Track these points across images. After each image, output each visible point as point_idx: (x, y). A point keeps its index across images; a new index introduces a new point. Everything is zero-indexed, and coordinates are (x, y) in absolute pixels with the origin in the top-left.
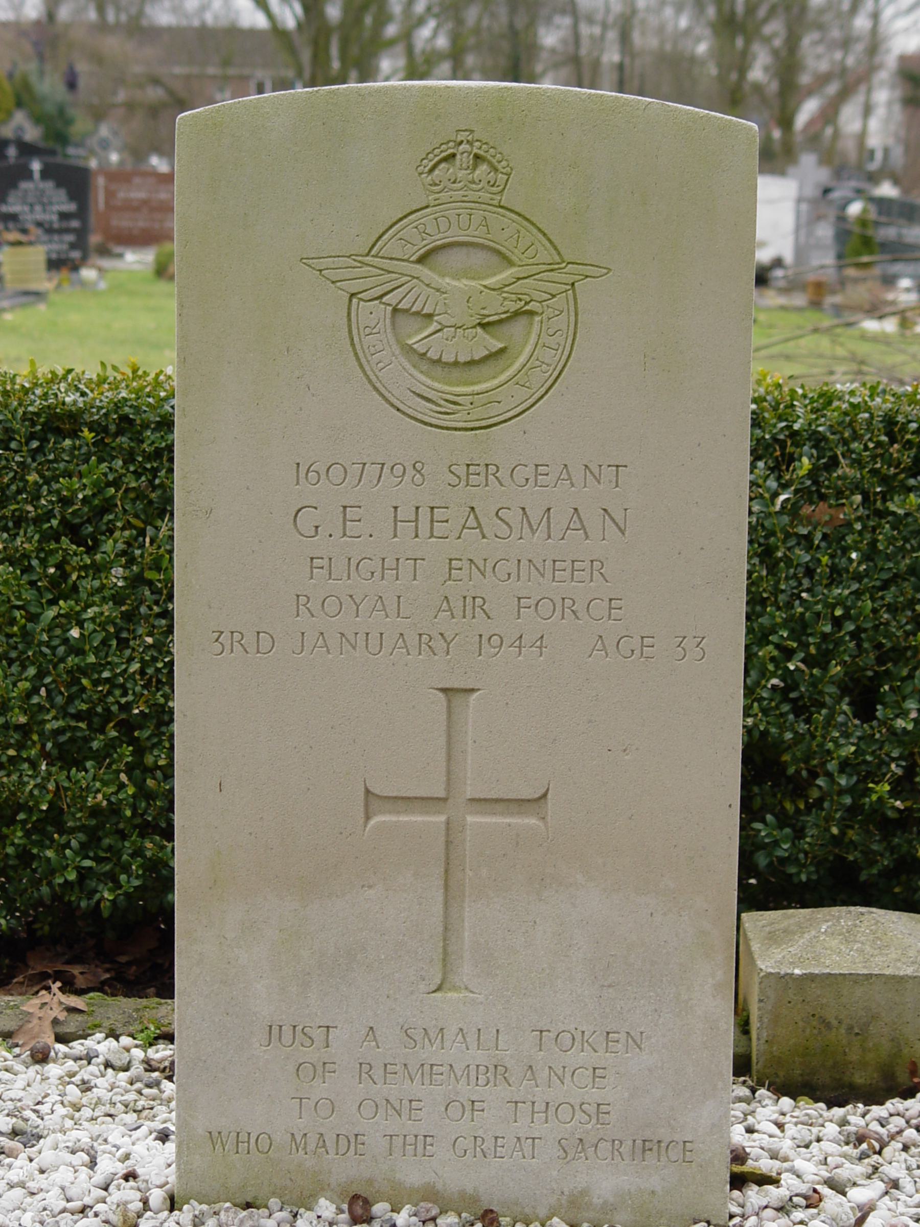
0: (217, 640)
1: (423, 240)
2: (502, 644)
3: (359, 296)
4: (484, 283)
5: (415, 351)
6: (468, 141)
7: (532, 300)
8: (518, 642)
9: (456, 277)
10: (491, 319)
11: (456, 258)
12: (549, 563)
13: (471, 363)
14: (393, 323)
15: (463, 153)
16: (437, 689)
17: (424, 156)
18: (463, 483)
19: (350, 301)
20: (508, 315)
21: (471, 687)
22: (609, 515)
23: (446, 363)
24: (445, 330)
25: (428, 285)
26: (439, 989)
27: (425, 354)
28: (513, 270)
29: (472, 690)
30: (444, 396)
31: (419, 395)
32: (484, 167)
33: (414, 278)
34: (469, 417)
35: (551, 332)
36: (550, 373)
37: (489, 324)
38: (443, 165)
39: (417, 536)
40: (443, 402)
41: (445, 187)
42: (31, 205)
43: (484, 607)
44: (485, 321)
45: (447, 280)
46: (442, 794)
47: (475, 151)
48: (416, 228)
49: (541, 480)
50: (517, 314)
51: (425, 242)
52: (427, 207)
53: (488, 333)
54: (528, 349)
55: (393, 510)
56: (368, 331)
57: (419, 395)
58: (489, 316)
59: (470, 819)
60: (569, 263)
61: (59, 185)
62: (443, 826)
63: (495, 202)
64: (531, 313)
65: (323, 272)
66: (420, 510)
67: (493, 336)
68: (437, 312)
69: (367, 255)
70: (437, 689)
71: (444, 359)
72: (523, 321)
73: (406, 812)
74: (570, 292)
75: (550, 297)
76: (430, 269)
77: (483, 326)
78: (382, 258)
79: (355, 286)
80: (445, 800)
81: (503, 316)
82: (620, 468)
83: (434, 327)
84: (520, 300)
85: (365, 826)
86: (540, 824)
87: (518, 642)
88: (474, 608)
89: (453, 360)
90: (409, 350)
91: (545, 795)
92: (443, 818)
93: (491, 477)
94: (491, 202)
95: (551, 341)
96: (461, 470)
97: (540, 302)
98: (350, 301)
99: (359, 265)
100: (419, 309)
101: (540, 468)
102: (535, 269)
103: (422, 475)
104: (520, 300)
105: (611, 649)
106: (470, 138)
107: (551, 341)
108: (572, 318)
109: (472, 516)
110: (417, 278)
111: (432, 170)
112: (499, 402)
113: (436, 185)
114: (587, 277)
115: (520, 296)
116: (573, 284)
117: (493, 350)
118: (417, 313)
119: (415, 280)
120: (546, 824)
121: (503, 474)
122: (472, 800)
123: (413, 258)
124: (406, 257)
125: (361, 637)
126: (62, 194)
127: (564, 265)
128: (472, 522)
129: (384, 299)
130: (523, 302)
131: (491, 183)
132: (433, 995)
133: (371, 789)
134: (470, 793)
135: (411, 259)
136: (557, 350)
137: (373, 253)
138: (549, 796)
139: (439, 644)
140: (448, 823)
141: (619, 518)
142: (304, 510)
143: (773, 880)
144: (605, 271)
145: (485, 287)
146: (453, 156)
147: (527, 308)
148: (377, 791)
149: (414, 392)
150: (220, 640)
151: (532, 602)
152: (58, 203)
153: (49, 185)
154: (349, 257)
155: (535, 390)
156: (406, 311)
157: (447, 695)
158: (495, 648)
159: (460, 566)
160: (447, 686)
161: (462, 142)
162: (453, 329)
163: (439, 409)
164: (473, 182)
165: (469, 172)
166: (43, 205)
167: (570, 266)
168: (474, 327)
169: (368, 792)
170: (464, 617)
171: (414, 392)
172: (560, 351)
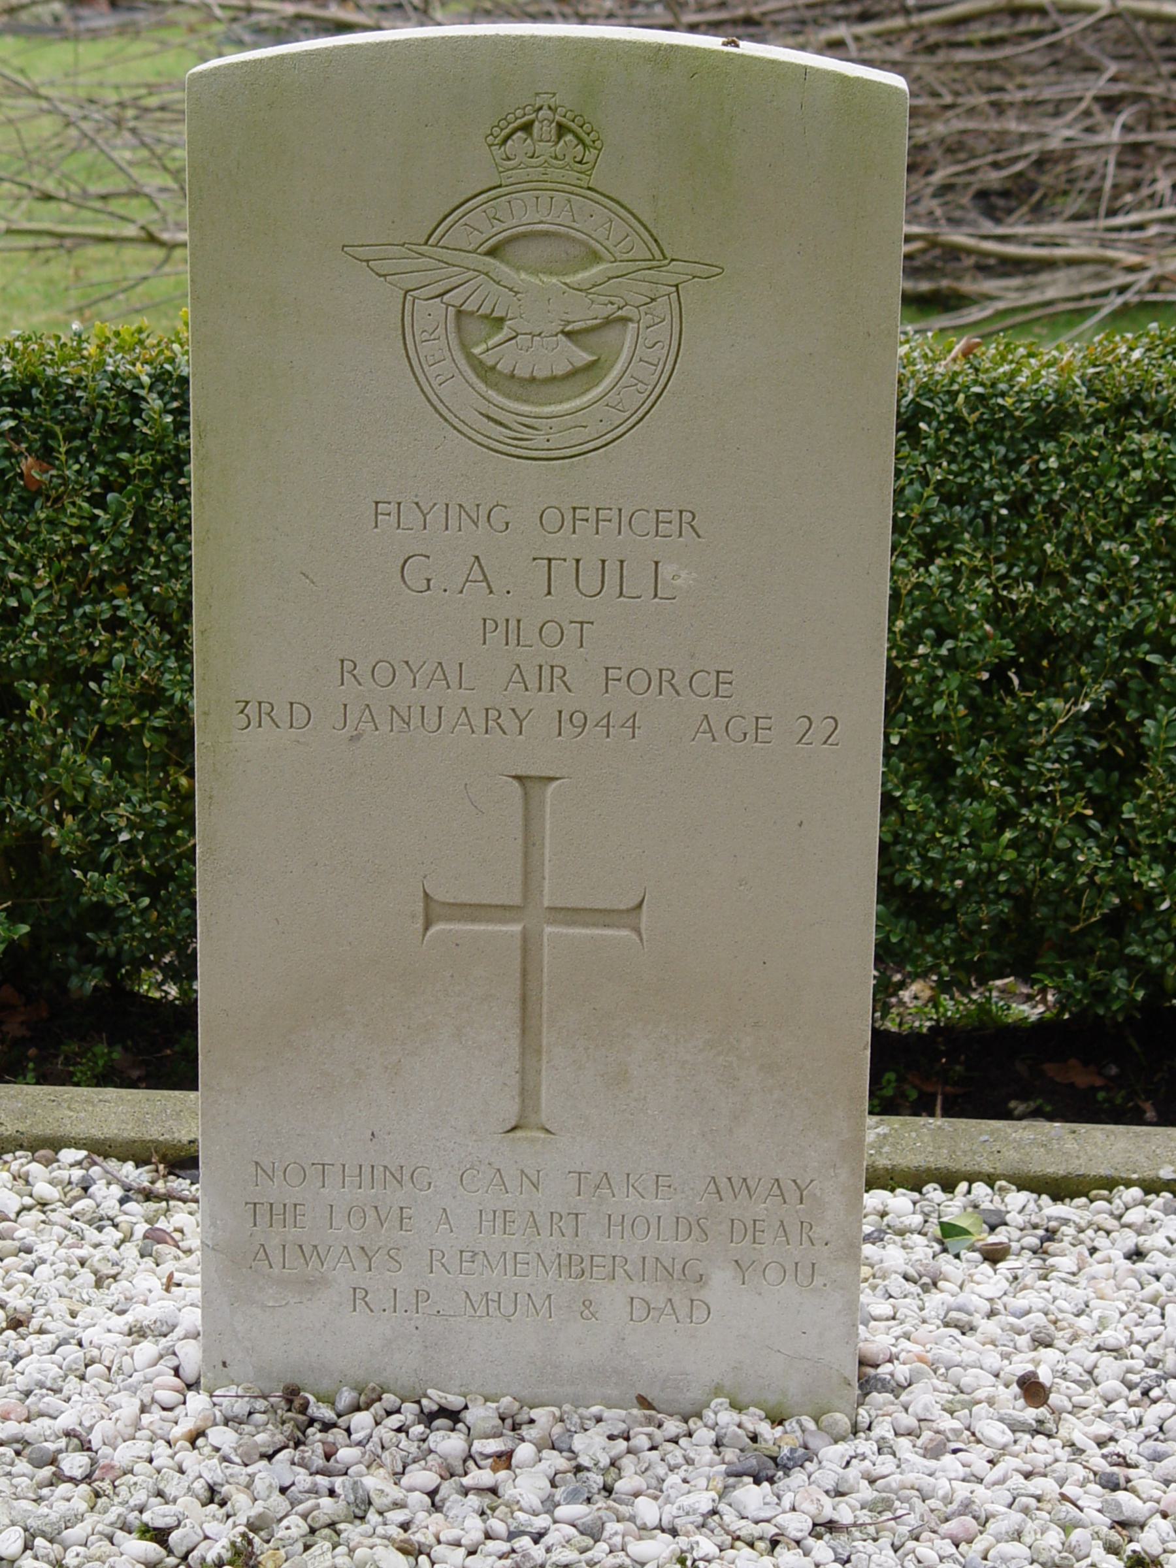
0: (242, 712)
2: (585, 724)
6: (550, 108)
9: (535, 272)
11: (533, 252)
13: (553, 379)
14: (459, 328)
15: (542, 122)
19: (405, 297)
20: (598, 321)
22: (480, 566)
27: (493, 368)
28: (601, 267)
29: (552, 779)
30: (520, 419)
32: (569, 137)
35: (649, 343)
36: (648, 393)
38: (519, 134)
39: (549, 593)
40: (515, 426)
43: (565, 679)
44: (568, 328)
46: (517, 900)
47: (557, 118)
50: (608, 322)
51: (495, 230)
52: (500, 186)
53: (576, 343)
56: (425, 336)
59: (548, 929)
62: (518, 943)
64: (625, 320)
65: (371, 263)
66: (625, 564)
69: (426, 243)
76: (502, 261)
77: (568, 334)
78: (442, 247)
79: (410, 281)
81: (590, 323)
85: (424, 936)
86: (634, 936)
92: (517, 928)
98: (405, 297)
102: (632, 266)
104: (612, 304)
106: (552, 102)
110: (486, 274)
111: (505, 141)
113: (509, 159)
116: (677, 286)
120: (640, 935)
122: (550, 909)
127: (666, 262)
128: (476, 574)
129: (446, 297)
131: (578, 159)
133: (431, 894)
134: (546, 904)
136: (656, 366)
139: (508, 720)
140: (525, 937)
145: (565, 284)
147: (620, 313)
149: (481, 414)
151: (623, 674)
154: (403, 245)
156: (472, 313)
159: (515, 623)
161: (540, 108)
169: (426, 895)
170: (540, 689)
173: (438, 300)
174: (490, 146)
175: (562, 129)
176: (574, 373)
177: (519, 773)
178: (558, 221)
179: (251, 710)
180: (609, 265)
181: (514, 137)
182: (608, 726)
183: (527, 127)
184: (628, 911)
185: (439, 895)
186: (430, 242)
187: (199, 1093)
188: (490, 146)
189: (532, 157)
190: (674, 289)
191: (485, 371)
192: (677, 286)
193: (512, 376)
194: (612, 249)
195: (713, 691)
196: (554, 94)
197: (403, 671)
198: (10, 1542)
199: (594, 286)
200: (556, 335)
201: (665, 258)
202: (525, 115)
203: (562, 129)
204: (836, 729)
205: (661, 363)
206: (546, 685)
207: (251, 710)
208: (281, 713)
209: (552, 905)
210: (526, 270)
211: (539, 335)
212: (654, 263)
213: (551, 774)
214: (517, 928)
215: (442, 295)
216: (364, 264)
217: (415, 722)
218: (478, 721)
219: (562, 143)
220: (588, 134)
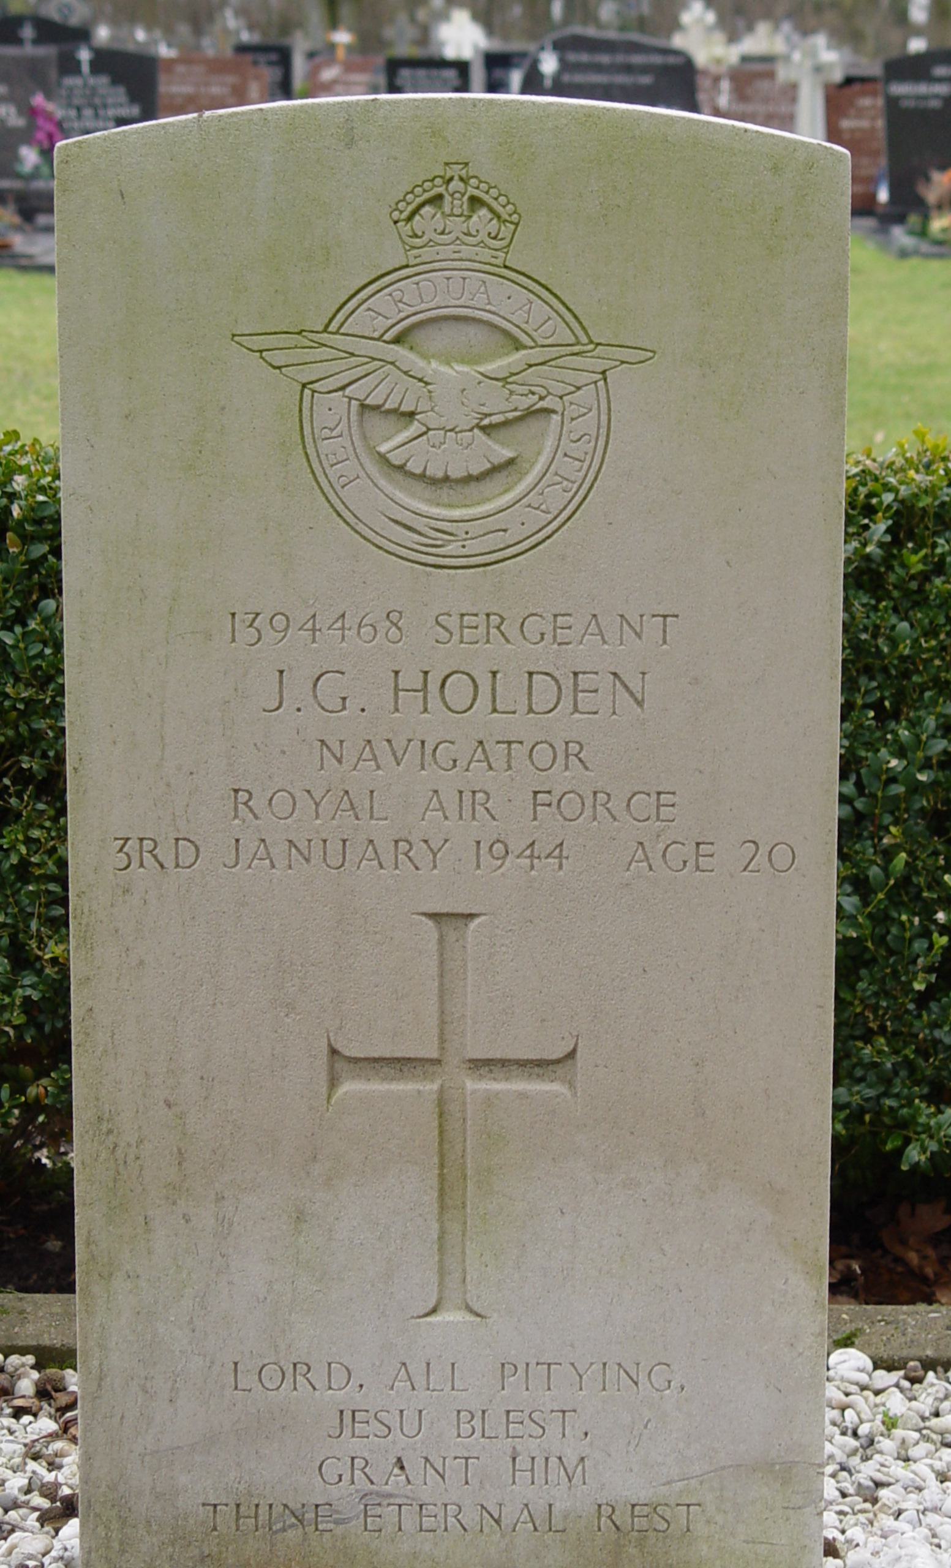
1: (400, 311)
4: (482, 370)
5: (387, 461)
7: (429, 429)
8: (558, 850)
10: (495, 419)
13: (469, 479)
16: (425, 914)
17: (410, 190)
18: (456, 638)
21: (469, 912)
24: (431, 433)
25: (406, 373)
26: (434, 1311)
29: (471, 916)
30: (433, 523)
31: (396, 522)
34: (465, 551)
42: (79, 109)
44: (486, 422)
45: (434, 364)
47: (471, 191)
48: (390, 295)
49: (562, 634)
50: (531, 413)
51: (402, 315)
53: (485, 433)
54: (543, 460)
55: (393, 674)
57: (396, 522)
58: (491, 415)
59: (470, 1085)
61: (116, 81)
63: (499, 262)
67: (497, 441)
68: (419, 410)
69: (325, 330)
70: (425, 914)
72: (534, 426)
75: (573, 389)
77: (483, 429)
78: (343, 334)
80: (437, 1062)
81: (510, 415)
82: (669, 619)
83: (415, 428)
84: (533, 393)
86: (569, 1094)
87: (558, 850)
88: (594, 806)
90: (383, 458)
91: (572, 1054)
92: (435, 1087)
93: (493, 631)
94: (493, 261)
95: (576, 450)
96: (453, 622)
99: (316, 345)
100: (396, 405)
101: (559, 618)
102: (555, 351)
103: (399, 629)
104: (533, 393)
105: (657, 862)
106: (463, 173)
107: (576, 450)
108: (604, 418)
110: (392, 363)
111: (410, 218)
113: (416, 236)
114: (623, 362)
117: (496, 461)
118: (394, 411)
119: (389, 366)
123: (387, 337)
125: (317, 846)
126: (120, 94)
129: (348, 391)
130: (536, 397)
131: (493, 235)
132: (428, 1319)
133: (338, 1046)
135: (386, 337)
137: (333, 327)
138: (579, 1054)
139: (420, 851)
141: (635, 685)
144: (651, 354)
146: (440, 197)
147: (541, 405)
148: (347, 1053)
149: (390, 519)
152: (116, 105)
153: (103, 80)
154: (299, 333)
156: (376, 408)
157: (436, 921)
158: (498, 859)
160: (437, 910)
161: (451, 179)
162: (442, 432)
164: (468, 234)
165: (463, 219)
166: (95, 108)
167: (600, 347)
168: (471, 430)
169: (334, 1052)
171: (390, 519)
172: (587, 463)
173: (340, 393)
176: (495, 469)
181: (423, 211)
186: (330, 329)
188: (396, 222)
190: (600, 376)
192: (604, 372)
194: (534, 334)
196: (467, 164)
203: (475, 202)
205: (589, 458)
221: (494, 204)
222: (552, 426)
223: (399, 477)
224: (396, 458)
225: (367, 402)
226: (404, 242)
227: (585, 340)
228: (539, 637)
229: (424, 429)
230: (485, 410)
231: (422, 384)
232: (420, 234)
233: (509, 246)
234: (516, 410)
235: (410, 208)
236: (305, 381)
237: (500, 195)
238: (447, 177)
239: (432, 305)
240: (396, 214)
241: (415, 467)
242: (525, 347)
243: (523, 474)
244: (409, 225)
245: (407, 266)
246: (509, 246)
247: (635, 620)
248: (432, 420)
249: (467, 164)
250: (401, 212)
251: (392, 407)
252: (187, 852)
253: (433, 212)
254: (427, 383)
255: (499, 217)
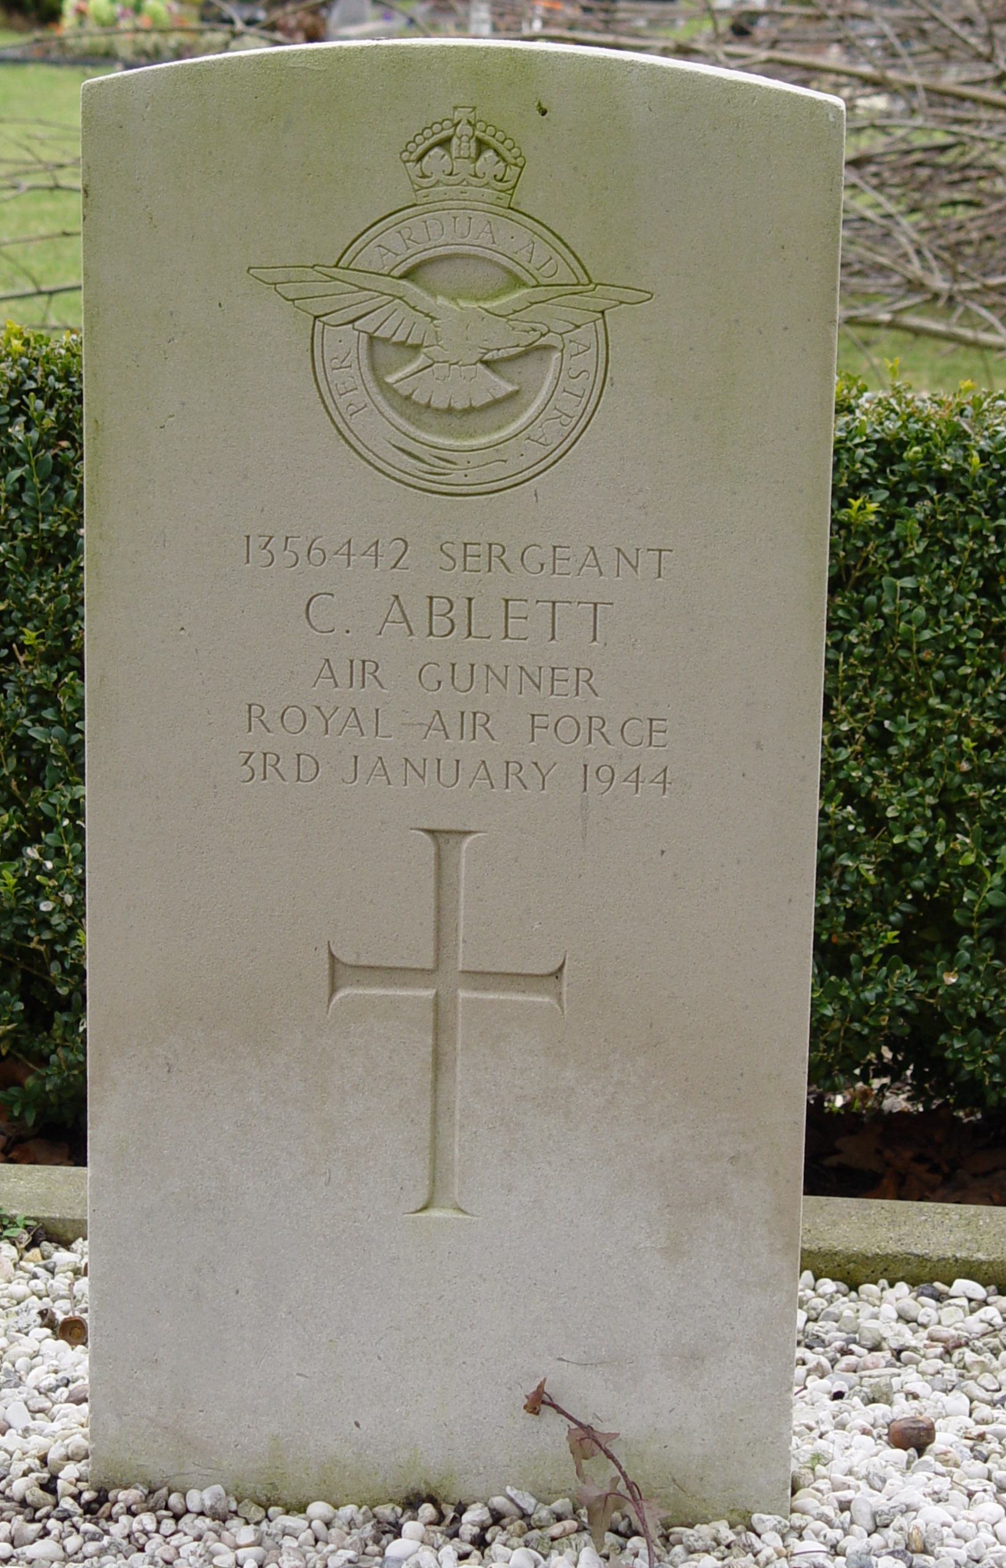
3: (322, 319)
4: (486, 306)
6: (469, 122)
7: (549, 331)
10: (502, 353)
12: (546, 673)
13: (469, 411)
20: (519, 349)
22: (400, 604)
23: (437, 410)
25: (413, 308)
26: (424, 1208)
27: (408, 398)
29: (470, 833)
32: (489, 154)
33: (395, 297)
35: (573, 374)
37: (495, 362)
38: (436, 150)
41: (438, 182)
44: (486, 357)
45: (441, 300)
46: (430, 966)
49: (561, 567)
50: (530, 351)
53: (494, 371)
59: (462, 994)
60: (597, 285)
66: (473, 602)
67: (502, 377)
69: (336, 266)
71: (434, 404)
72: (531, 364)
73: (404, 985)
74: (601, 321)
77: (486, 363)
89: (446, 406)
90: (386, 389)
92: (429, 993)
94: (462, 196)
97: (561, 334)
100: (403, 339)
104: (534, 330)
109: (396, 604)
110: (400, 298)
111: (420, 159)
112: (505, 461)
114: (621, 303)
115: (533, 325)
116: (603, 312)
118: (402, 344)
119: (397, 301)
121: (510, 557)
122: (462, 972)
124: (385, 271)
125: (431, 766)
127: (592, 286)
128: (396, 614)
129: (357, 323)
131: (499, 177)
132: (419, 1214)
134: (460, 969)
142: (313, 603)
143: (909, 1073)
145: (486, 310)
147: (543, 341)
148: (344, 959)
149: (394, 446)
150: (249, 762)
154: (313, 267)
155: (553, 446)
156: (386, 340)
163: (426, 467)
164: (475, 176)
167: (599, 287)
169: (332, 956)
171: (394, 446)
172: (584, 400)
173: (350, 326)
174: (405, 162)
175: (482, 145)
176: (496, 403)
177: (434, 826)
178: (476, 242)
179: (256, 761)
180: (531, 290)
181: (432, 153)
182: (664, 782)
183: (444, 143)
184: (551, 975)
185: (346, 956)
186: (341, 264)
187: (88, 1171)
188: (405, 162)
189: (450, 174)
190: (600, 315)
191: (405, 403)
192: (603, 312)
193: (428, 406)
194: (535, 273)
195: (646, 740)
196: (474, 108)
197: (312, 714)
198: (2, 1549)
199: (515, 312)
200: (475, 364)
201: (591, 282)
202: (443, 129)
203: (482, 145)
204: (451, 632)
205: (587, 393)
206: (357, 678)
207: (256, 761)
208: (287, 765)
209: (466, 968)
210: (445, 295)
211: (456, 363)
212: (580, 288)
213: (467, 829)
214: (429, 993)
215: (353, 321)
216: (290, 303)
217: (431, 775)
218: (498, 775)
219: (482, 159)
220: (510, 150)
221: (502, 149)
222: (553, 362)
223: (426, 417)
224: (404, 389)
225: (376, 334)
226: (412, 183)
227: (585, 280)
228: (539, 567)
229: (431, 362)
230: (487, 344)
231: (429, 319)
232: (480, 174)
233: (514, 187)
234: (518, 346)
235: (420, 150)
236: (316, 314)
237: (414, 141)
238: (456, 121)
239: (442, 241)
240: (405, 155)
241: (420, 397)
242: (525, 285)
243: (526, 406)
244: (418, 166)
245: (415, 205)
246: (514, 187)
247: (632, 556)
248: (434, 351)
249: (474, 108)
250: (411, 153)
251: (415, 342)
252: (308, 769)
253: (443, 153)
254: (433, 318)
255: (504, 160)
